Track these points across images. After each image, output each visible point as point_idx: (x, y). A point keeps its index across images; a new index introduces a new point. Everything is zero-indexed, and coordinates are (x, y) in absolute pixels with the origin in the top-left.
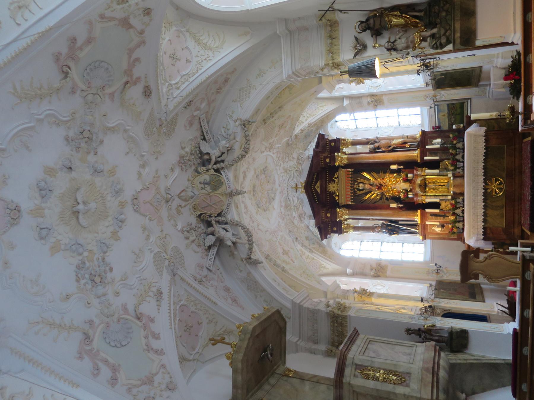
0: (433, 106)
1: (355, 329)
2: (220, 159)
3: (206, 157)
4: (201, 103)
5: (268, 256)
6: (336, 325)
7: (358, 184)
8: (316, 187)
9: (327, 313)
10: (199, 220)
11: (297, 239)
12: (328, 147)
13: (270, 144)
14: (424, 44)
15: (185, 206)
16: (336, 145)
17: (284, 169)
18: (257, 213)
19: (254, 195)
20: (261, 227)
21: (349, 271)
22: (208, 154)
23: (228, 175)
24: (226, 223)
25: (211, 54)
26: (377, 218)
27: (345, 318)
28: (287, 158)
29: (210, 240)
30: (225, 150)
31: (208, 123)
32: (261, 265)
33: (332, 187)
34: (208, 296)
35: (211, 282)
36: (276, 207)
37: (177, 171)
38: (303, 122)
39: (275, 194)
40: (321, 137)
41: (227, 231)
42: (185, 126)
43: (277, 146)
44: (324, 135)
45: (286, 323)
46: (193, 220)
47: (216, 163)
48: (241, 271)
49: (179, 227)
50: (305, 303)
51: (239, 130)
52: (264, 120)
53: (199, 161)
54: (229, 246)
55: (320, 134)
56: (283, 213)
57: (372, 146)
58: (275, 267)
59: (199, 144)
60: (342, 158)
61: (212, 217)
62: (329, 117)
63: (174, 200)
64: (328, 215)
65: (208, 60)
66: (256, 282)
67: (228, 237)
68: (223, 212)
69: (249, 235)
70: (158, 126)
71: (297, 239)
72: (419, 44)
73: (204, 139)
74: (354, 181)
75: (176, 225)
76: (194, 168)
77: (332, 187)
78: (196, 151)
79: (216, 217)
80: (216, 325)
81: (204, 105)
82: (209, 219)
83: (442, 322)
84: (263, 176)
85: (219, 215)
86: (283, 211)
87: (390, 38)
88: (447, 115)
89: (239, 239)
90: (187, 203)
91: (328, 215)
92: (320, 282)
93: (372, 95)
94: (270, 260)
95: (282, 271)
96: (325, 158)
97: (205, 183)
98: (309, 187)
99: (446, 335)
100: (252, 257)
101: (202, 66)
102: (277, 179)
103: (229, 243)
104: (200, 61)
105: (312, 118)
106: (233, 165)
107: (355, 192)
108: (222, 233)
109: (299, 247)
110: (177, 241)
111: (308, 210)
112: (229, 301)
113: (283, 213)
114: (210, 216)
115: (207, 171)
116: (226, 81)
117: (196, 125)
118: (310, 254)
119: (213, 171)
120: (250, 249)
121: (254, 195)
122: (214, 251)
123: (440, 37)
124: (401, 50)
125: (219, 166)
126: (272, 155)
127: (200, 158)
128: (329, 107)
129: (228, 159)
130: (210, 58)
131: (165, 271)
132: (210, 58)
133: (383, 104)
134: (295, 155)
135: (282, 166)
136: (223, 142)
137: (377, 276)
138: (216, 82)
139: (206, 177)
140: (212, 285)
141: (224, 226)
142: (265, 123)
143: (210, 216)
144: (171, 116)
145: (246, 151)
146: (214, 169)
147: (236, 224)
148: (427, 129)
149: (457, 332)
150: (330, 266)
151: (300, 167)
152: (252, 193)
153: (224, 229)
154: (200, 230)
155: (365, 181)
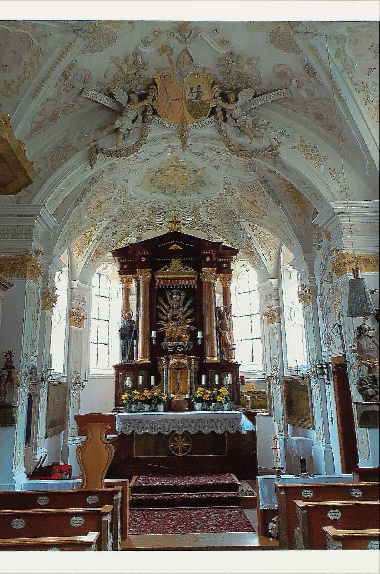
0: (266, 377)
1: (11, 285)
2: (228, 116)
3: (232, 97)
4: (307, 90)
5: (97, 181)
6: (13, 263)
7: (179, 294)
9: (28, 251)
11: (115, 221)
12: (219, 259)
13: (234, 189)
14: (365, 370)
15: (170, 61)
16: (224, 270)
17: (200, 207)
18: (150, 169)
19: (173, 166)
20: (132, 173)
21: (75, 283)
22: (237, 100)
23: (206, 128)
24: (143, 121)
26: (138, 314)
27: (22, 274)
29: (122, 97)
30: (240, 123)
31: (276, 101)
32: (89, 167)
33: (176, 263)
37: (221, 51)
39: (170, 195)
40: (234, 252)
41: (133, 121)
42: (279, 65)
43: (229, 198)
44: (237, 256)
45: (13, 194)
46: (150, 73)
47: (223, 110)
48: (79, 139)
50: (38, 221)
51: (265, 143)
52: (266, 181)
53: (228, 86)
54: (114, 123)
55: (237, 251)
57: (222, 309)
58: (83, 190)
59: (250, 87)
60: (209, 274)
61: (153, 101)
62: (257, 262)
63: (181, 42)
64: (143, 259)
65: (367, 101)
66: (66, 159)
67: (124, 123)
68: (158, 118)
69: (128, 152)
72: (365, 364)
73: (256, 96)
74: (182, 289)
75: (146, 43)
76: (220, 78)
77: (176, 263)
78: (242, 83)
81: (304, 94)
82: (149, 97)
83: (24, 394)
84: (193, 178)
85: (155, 112)
86: (148, 205)
87: (372, 330)
88: (253, 390)
89: (124, 139)
90: (174, 64)
91: (143, 259)
93: (280, 311)
94: (91, 184)
95: (77, 199)
96: (211, 256)
99: (7, 401)
102: (186, 198)
103: (118, 124)
106: (220, 134)
107: (170, 290)
108: (131, 115)
109: (104, 223)
111: (149, 235)
112: (38, 119)
115: (214, 97)
116: (331, 128)
118: (95, 237)
119: (214, 106)
120: (110, 153)
121: (173, 166)
122: (106, 101)
123: (373, 388)
124: (358, 343)
126: (219, 192)
127: (231, 89)
128: (268, 262)
129: (229, 129)
133: (268, 323)
134: (214, 221)
136: (250, 121)
137: (70, 314)
139: (206, 96)
141: (140, 117)
142: (262, 183)
144: (299, 42)
145: (239, 151)
146: (216, 107)
147: (142, 136)
148: (241, 369)
149: (11, 414)
150: (80, 262)
151: (198, 228)
153: (136, 118)
154: (136, 82)
155: (182, 301)
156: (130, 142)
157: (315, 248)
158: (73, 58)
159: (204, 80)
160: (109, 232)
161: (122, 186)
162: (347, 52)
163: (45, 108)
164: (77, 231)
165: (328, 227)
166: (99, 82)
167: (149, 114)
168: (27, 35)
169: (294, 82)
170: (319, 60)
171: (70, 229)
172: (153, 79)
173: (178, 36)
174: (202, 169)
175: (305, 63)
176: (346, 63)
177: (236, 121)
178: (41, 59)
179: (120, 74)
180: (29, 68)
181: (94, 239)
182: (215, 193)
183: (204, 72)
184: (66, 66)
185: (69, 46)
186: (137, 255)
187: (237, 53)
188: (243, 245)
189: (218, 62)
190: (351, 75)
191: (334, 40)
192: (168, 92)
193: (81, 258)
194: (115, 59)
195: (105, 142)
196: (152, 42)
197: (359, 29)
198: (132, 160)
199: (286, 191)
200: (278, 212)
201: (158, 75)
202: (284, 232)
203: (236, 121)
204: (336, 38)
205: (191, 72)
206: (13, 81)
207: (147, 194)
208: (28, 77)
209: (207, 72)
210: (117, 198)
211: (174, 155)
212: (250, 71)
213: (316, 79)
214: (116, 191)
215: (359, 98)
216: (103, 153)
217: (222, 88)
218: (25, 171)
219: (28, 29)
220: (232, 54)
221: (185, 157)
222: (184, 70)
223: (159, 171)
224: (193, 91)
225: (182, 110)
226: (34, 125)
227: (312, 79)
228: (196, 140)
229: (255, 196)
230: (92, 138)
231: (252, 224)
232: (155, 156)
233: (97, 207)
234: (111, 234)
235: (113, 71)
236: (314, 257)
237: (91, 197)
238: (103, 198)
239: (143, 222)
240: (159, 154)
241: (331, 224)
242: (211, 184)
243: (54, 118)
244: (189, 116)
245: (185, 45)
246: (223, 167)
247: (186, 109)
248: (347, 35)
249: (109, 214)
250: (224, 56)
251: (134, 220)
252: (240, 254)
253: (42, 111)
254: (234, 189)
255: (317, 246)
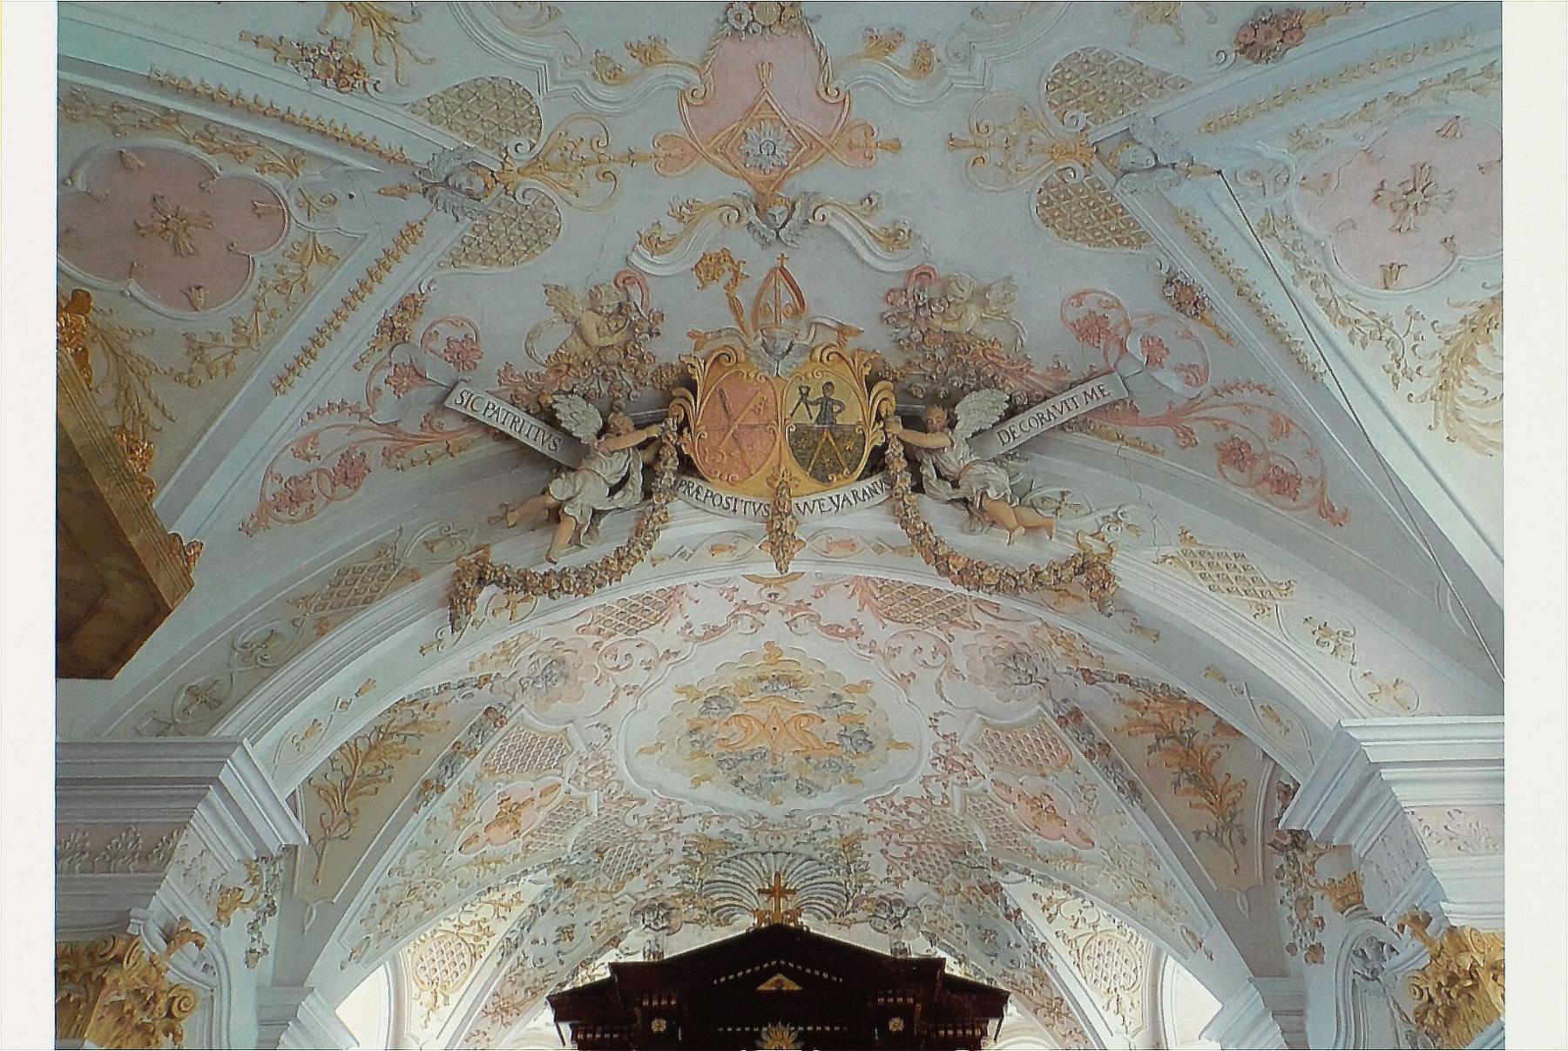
2: (928, 471)
3: (937, 415)
4: (1178, 369)
5: (500, 721)
8: (780, 976)
9: (124, 920)
10: (669, 377)
11: (569, 882)
13: (969, 758)
15: (735, 308)
17: (860, 835)
22: (952, 424)
23: (852, 514)
24: (647, 494)
25: (1421, 386)
28: (901, 852)
29: (582, 420)
34: (231, 90)
35: (387, 390)
36: (706, 791)
37: (893, 265)
38: (1050, 919)
40: (991, 1002)
41: (613, 490)
42: (1079, 297)
46: (670, 349)
48: (429, 545)
49: (643, 262)
50: (212, 808)
51: (1058, 548)
52: (1076, 715)
54: (545, 491)
56: (677, 828)
59: (991, 383)
64: (659, 1025)
65: (1397, 373)
67: (583, 492)
68: (697, 483)
70: (1098, 133)
71: (569, 882)
73: (1012, 412)
75: (654, 243)
76: (895, 361)
79: (678, 448)
80: (178, 378)
81: (1174, 383)
84: (833, 727)
85: (687, 466)
86: (688, 828)
92: (361, 956)
95: (426, 783)
96: (905, 1012)
97: (826, 403)
98: (778, 942)
100: (487, 591)
101: (1364, 345)
104: (1387, 334)
105: (1070, 960)
108: (609, 467)
109: (530, 890)
110: (591, 239)
112: (291, 467)
113: (677, 828)
114: (684, 425)
115: (879, 418)
116: (1284, 484)
117: (1082, 357)
118: (494, 941)
119: (879, 443)
121: (760, 680)
122: (530, 432)
125: (899, 465)
130: (1403, 381)
131: (450, 141)
132: (1403, 381)
134: (911, 889)
135: (871, 829)
138: (1281, 427)
139: (853, 412)
140: (374, 394)
141: (638, 479)
142: (1063, 722)
143: (684, 425)
144: (1138, 207)
147: (643, 534)
152: (770, 672)
153: (625, 480)
156: (594, 553)
157: (1297, 961)
158: (417, 274)
159: (842, 368)
160: (546, 928)
161: (590, 746)
162: (1300, 217)
163: (316, 434)
164: (417, 907)
165: (1351, 829)
166: (508, 366)
167: (668, 466)
168: (273, 191)
169: (1134, 345)
170: (1214, 257)
171: (392, 894)
172: (684, 371)
173: (754, 219)
174: (858, 688)
175: (1163, 272)
176: (1301, 255)
177: (955, 485)
178: (314, 273)
179: (577, 346)
180: (273, 300)
181: (489, 949)
182: (904, 780)
183: (841, 344)
184: (395, 300)
185: (411, 233)
186: (637, 1011)
187: (941, 270)
188: (1019, 976)
189: (886, 307)
190: (1324, 292)
191: (1251, 184)
192: (730, 404)
193: (435, 1026)
194: (555, 293)
195: (514, 551)
196: (674, 240)
197: (1326, 134)
198: (622, 650)
199: (1151, 749)
200: (1134, 827)
201: (699, 355)
202: (1164, 906)
203: (955, 485)
204: (1254, 175)
205: (803, 340)
206: (216, 338)
207: (678, 784)
208: (267, 325)
209: (852, 343)
210: (576, 793)
211: (763, 636)
212: (985, 331)
213: (1208, 324)
214: (570, 765)
215: (1369, 362)
216: (498, 583)
217: (905, 393)
218: (130, 554)
219: (274, 169)
220: (924, 274)
221: (798, 644)
222: (777, 332)
223: (716, 701)
224: (810, 399)
225: (774, 454)
226: (273, 488)
227: (1195, 327)
228: (824, 557)
229: (1043, 775)
230: (473, 540)
231: (1045, 893)
232: (698, 639)
233: (500, 821)
234: (553, 936)
235: (557, 337)
236: (1302, 997)
237: (479, 777)
238: (521, 786)
239: (668, 894)
240: (714, 632)
241: (1358, 820)
242: (893, 744)
243: (350, 473)
244: (796, 471)
245: (778, 250)
246: (928, 678)
247: (786, 451)
248: (1291, 160)
249: (545, 854)
250: (898, 283)
251: (637, 885)
252: (1011, 1010)
253: (304, 442)
254: (969, 758)
255: (1301, 953)
